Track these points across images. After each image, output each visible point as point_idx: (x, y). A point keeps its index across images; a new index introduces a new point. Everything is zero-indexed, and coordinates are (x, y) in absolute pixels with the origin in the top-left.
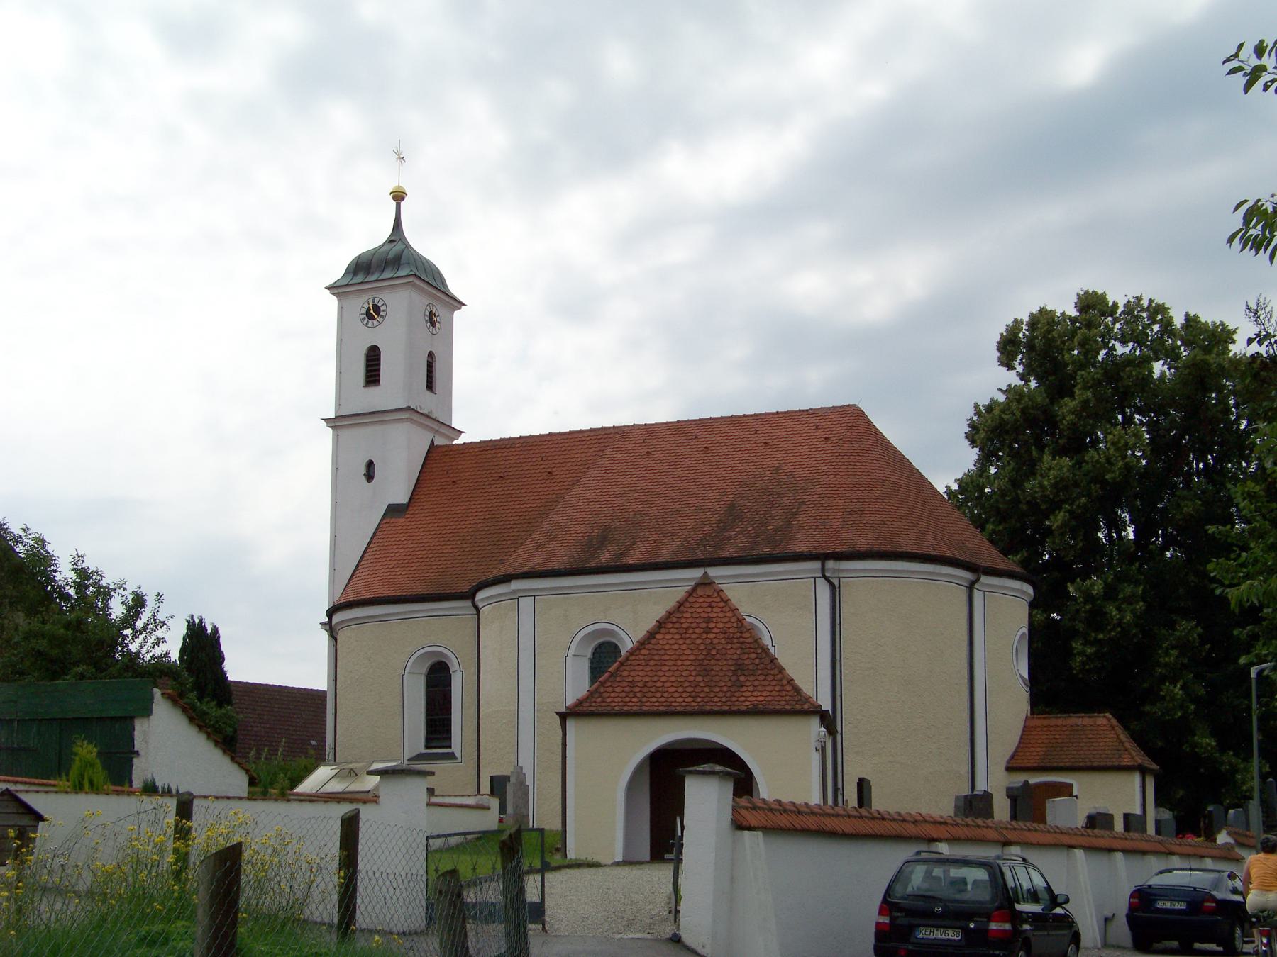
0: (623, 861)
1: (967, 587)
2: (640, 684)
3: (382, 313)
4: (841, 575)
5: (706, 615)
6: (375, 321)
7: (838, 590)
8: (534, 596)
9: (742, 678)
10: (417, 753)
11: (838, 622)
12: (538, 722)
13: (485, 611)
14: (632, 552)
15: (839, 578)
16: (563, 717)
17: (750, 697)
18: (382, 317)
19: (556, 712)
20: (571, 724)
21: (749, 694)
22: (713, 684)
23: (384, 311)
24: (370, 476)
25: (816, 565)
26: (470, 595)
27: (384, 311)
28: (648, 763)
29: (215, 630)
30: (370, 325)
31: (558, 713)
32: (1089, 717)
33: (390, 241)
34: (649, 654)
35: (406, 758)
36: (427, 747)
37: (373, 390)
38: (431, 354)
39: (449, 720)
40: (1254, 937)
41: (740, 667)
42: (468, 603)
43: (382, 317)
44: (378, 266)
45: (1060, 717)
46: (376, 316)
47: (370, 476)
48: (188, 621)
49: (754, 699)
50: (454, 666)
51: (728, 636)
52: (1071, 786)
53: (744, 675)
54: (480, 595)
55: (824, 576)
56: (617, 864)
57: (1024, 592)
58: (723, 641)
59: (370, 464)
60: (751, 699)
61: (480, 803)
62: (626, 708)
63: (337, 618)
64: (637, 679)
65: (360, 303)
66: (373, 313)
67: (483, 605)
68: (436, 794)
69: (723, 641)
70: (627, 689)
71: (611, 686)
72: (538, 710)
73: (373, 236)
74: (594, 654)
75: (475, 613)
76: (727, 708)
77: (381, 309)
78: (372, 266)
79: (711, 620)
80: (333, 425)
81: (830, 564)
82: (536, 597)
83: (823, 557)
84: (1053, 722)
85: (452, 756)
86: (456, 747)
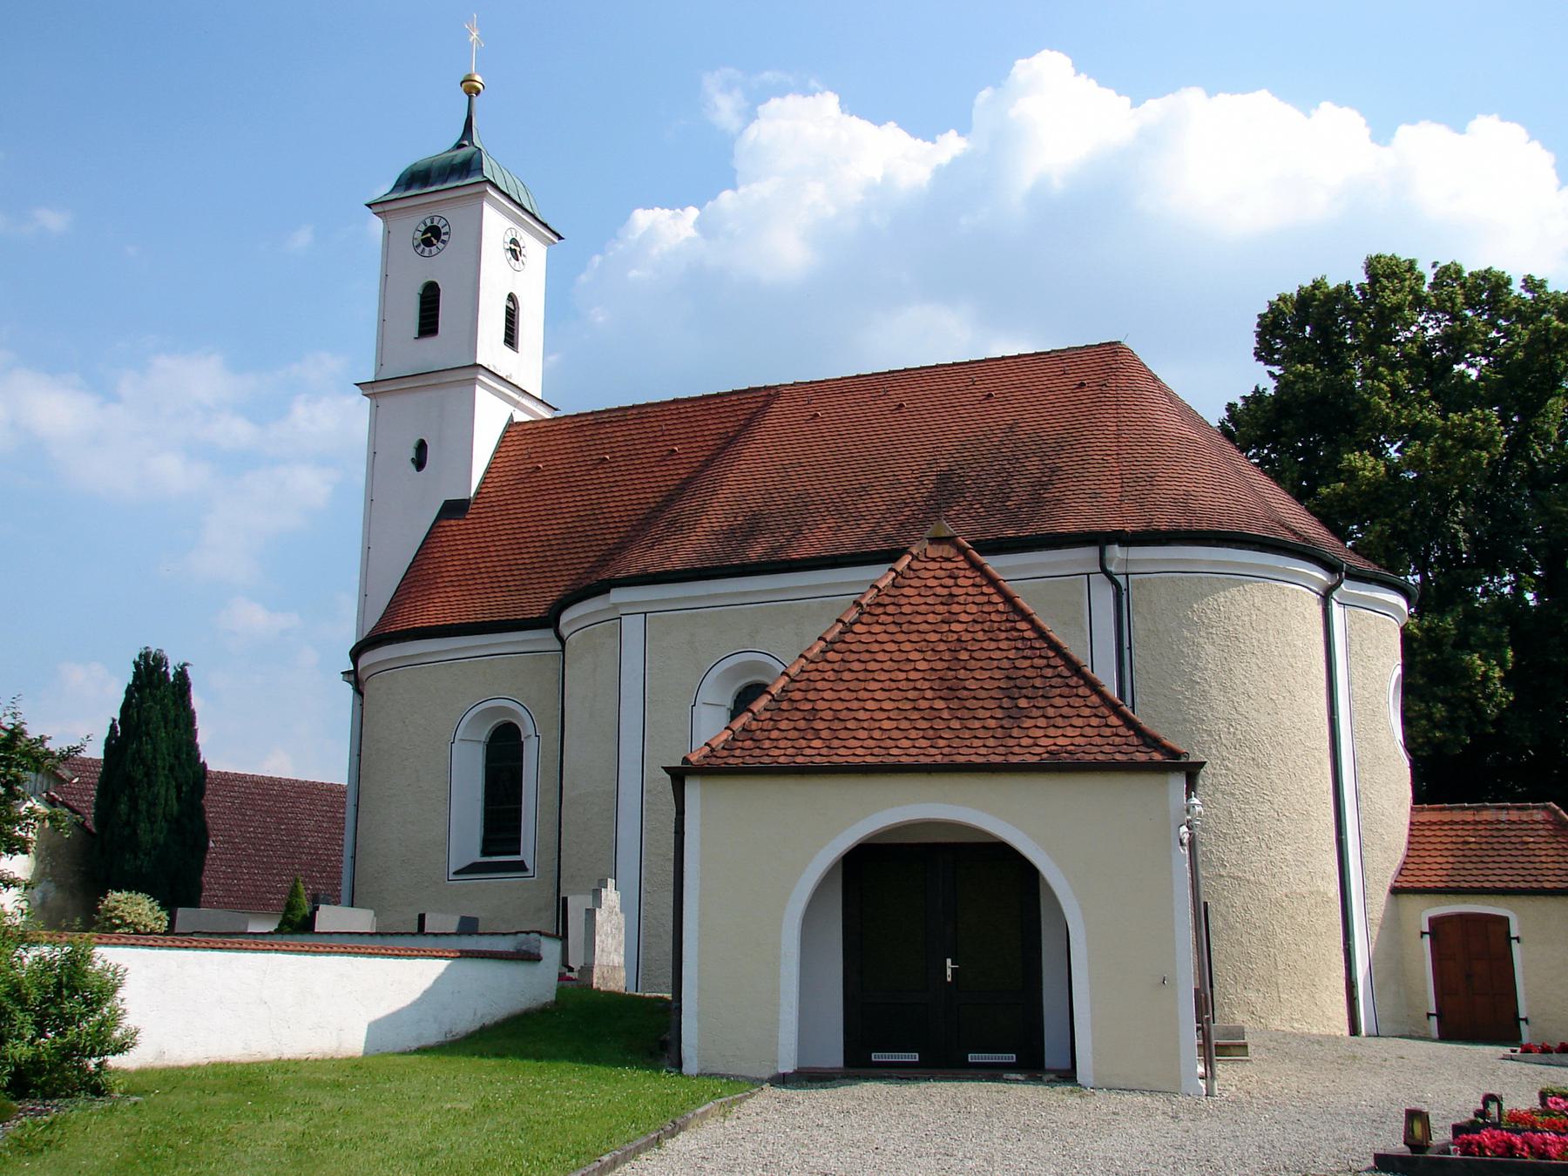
0: (795, 1072)
1: (1321, 595)
2: (828, 715)
3: (443, 237)
4: (1130, 570)
5: (945, 592)
6: (434, 248)
7: (1125, 593)
8: (645, 613)
9: (1023, 703)
10: (468, 862)
11: (1126, 644)
12: (647, 810)
13: (572, 641)
14: (795, 544)
15: (1127, 575)
16: (679, 776)
17: (1040, 739)
18: (444, 242)
19: (663, 767)
20: (694, 790)
21: (1039, 733)
22: (966, 714)
23: (446, 234)
24: (420, 462)
25: (1091, 553)
26: (550, 621)
27: (446, 234)
28: (841, 865)
29: (182, 675)
30: (419, 251)
31: (667, 769)
32: (1519, 809)
33: (459, 146)
34: (842, 660)
35: (452, 870)
36: (485, 853)
37: (428, 342)
38: (511, 297)
39: (519, 811)
40: (952, 968)
41: (1013, 687)
42: (550, 633)
43: (444, 242)
44: (439, 175)
45: (1468, 808)
46: (435, 241)
47: (420, 462)
48: (137, 665)
49: (1051, 741)
50: (527, 729)
51: (989, 627)
52: (1505, 921)
53: (1026, 697)
54: (565, 617)
55: (1104, 571)
56: (781, 1080)
57: (1396, 608)
58: (980, 636)
59: (422, 447)
60: (1043, 741)
61: (524, 948)
62: (800, 759)
63: (366, 659)
64: (821, 705)
65: (413, 225)
66: (432, 236)
67: (569, 633)
68: (316, 930)
69: (980, 636)
70: (802, 724)
71: (771, 719)
72: (647, 791)
73: (437, 144)
74: (735, 701)
75: (560, 648)
76: (998, 759)
77: (443, 231)
78: (432, 175)
79: (956, 599)
80: (371, 392)
81: (1116, 552)
82: (648, 615)
83: (1100, 540)
84: (1487, 815)
85: (520, 867)
86: (527, 854)
